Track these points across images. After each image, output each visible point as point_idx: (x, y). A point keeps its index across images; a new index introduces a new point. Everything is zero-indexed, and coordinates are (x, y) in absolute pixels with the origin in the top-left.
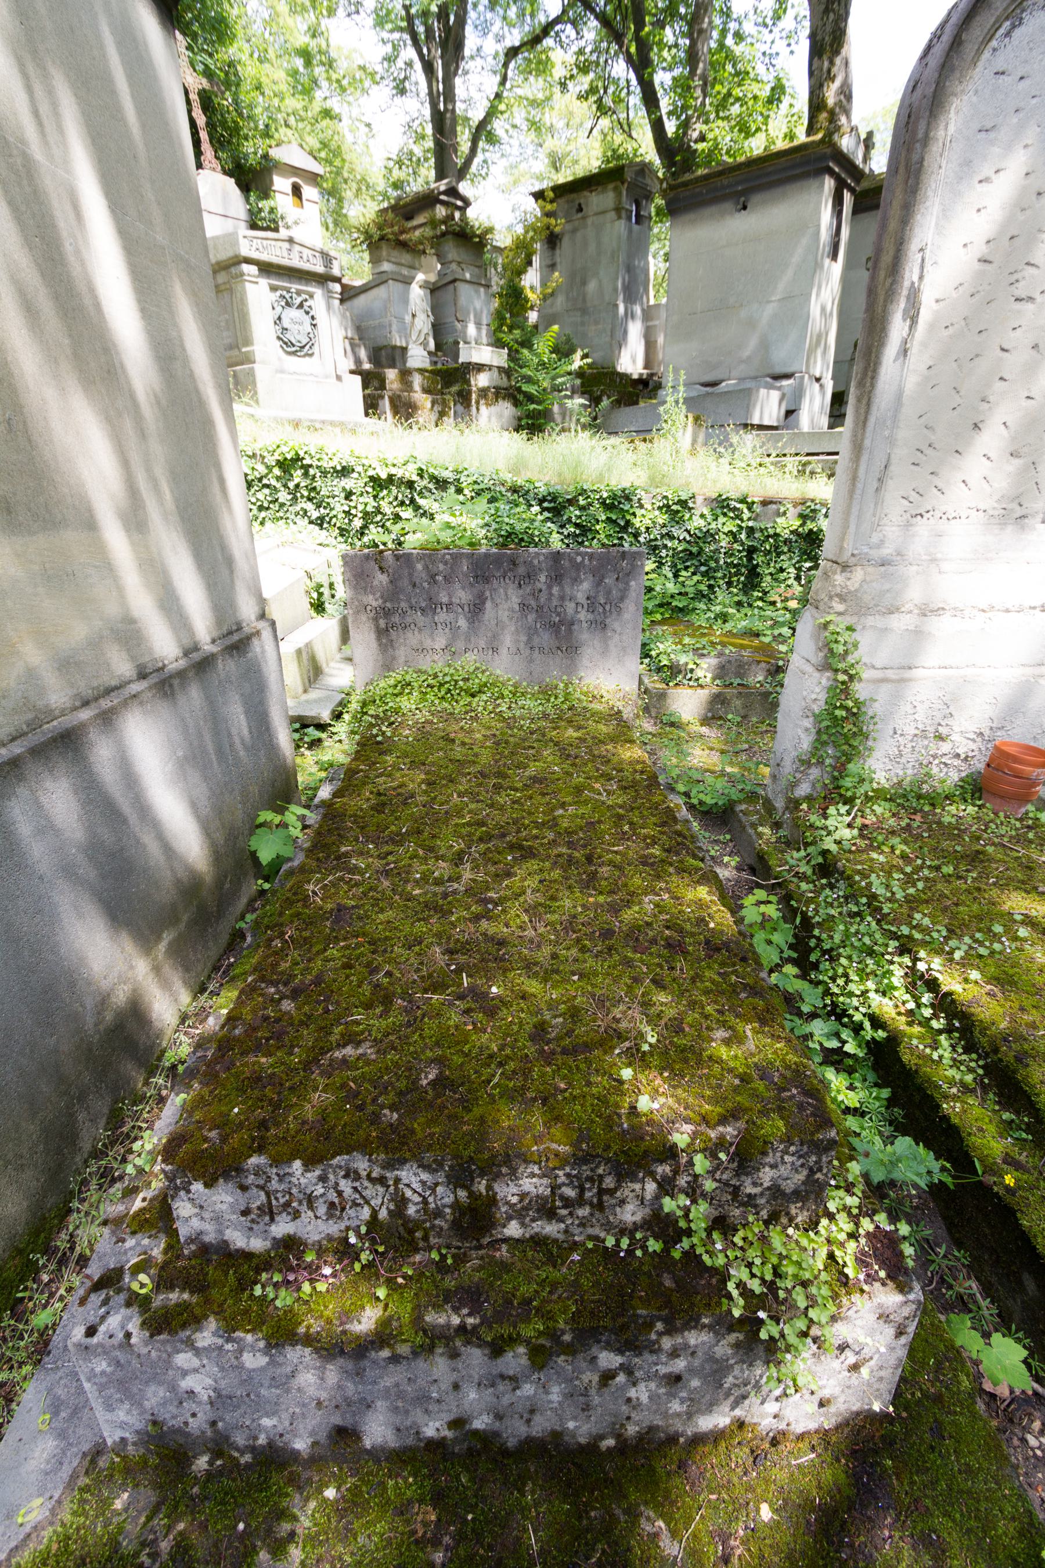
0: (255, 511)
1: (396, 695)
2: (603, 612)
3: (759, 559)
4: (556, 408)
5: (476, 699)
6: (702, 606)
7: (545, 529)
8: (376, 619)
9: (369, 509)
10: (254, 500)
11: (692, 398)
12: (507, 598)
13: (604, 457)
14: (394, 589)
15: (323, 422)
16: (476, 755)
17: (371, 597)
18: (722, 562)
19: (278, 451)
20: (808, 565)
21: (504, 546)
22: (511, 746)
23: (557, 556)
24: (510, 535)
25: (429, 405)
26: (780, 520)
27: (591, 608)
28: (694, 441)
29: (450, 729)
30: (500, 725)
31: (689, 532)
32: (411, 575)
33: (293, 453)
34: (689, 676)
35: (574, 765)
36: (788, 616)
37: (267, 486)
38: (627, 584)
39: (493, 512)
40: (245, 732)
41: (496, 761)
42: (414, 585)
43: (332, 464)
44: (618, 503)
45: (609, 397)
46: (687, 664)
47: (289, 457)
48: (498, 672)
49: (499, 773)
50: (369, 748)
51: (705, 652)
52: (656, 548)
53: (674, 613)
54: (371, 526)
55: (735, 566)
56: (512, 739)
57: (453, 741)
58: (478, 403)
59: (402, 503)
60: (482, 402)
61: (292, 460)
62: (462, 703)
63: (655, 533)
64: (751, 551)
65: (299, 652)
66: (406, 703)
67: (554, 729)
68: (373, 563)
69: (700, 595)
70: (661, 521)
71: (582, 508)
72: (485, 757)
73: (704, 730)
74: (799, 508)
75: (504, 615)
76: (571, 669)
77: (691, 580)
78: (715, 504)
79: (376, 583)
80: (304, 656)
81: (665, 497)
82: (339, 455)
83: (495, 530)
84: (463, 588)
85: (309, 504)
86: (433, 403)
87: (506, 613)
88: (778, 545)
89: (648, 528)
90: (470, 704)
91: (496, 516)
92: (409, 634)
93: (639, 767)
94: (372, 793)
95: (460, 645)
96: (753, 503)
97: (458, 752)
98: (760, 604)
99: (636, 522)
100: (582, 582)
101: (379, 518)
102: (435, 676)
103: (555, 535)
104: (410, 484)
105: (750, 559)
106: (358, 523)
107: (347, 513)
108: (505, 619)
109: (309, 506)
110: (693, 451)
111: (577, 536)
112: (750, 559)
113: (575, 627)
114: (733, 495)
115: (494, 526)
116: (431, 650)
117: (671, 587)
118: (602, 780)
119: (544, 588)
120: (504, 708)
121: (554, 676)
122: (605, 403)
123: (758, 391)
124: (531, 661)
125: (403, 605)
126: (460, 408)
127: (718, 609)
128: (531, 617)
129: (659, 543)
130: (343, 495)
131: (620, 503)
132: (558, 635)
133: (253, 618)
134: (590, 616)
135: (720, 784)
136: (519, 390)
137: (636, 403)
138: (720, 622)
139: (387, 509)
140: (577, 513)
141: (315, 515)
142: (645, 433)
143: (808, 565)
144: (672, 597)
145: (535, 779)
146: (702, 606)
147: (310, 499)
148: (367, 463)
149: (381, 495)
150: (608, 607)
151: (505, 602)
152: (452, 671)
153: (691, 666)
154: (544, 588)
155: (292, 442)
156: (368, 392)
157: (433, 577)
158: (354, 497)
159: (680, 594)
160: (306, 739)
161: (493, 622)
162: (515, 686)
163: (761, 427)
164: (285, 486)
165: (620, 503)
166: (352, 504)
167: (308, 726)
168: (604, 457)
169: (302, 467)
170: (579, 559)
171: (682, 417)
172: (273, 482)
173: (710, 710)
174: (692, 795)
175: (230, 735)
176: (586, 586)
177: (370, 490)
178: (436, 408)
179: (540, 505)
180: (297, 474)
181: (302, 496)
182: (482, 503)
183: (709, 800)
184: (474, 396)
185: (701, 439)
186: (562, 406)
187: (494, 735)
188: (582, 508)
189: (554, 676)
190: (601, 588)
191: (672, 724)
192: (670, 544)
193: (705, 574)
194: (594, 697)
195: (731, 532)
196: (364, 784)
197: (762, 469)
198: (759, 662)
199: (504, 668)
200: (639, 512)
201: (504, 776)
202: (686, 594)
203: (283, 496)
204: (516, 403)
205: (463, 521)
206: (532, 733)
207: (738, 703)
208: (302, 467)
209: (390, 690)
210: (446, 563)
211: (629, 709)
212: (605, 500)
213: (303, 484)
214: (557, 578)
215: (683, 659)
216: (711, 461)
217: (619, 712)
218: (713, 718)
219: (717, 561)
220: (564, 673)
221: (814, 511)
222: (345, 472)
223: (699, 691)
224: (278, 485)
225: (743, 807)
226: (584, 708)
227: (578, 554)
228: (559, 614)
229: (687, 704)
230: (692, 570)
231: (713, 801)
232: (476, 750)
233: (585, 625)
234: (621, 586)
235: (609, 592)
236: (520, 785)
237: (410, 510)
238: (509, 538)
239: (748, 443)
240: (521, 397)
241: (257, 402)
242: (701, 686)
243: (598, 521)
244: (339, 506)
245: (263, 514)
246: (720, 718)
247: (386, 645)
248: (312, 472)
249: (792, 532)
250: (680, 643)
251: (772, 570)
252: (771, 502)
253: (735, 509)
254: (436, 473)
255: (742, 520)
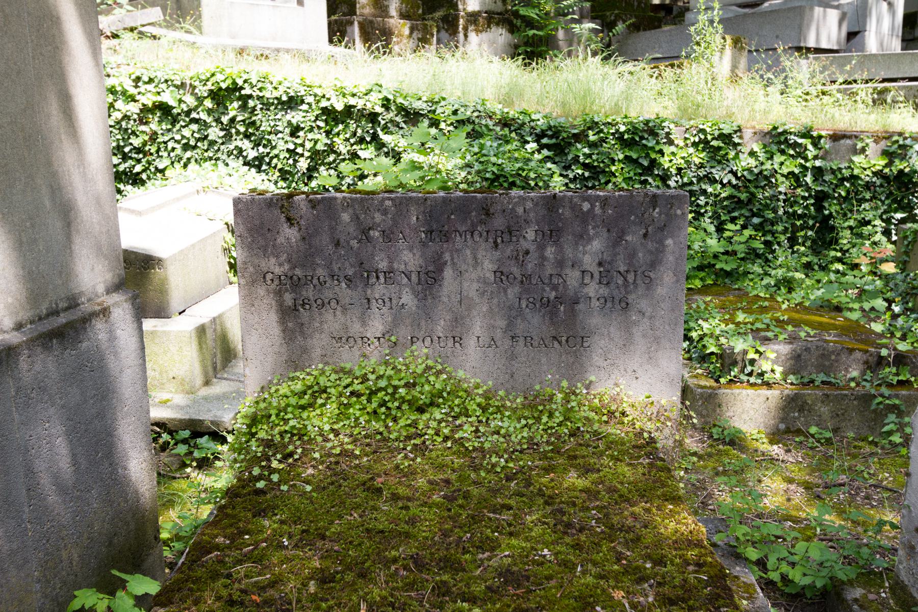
0: (179, 151)
1: (303, 408)
2: (623, 287)
3: (831, 208)
4: (561, 34)
5: (426, 416)
6: (757, 269)
7: (544, 171)
8: (279, 293)
9: (320, 147)
10: (178, 137)
11: (729, 19)
12: (476, 263)
13: (620, 86)
14: (305, 247)
15: (278, 50)
16: (412, 521)
17: (273, 260)
18: (781, 212)
19: (213, 80)
20: (899, 216)
21: (489, 190)
22: (476, 501)
23: (553, 201)
24: (497, 177)
25: (407, 31)
26: (857, 159)
27: (605, 278)
28: (734, 67)
29: (378, 468)
30: (458, 462)
31: (734, 174)
32: (332, 229)
33: (229, 82)
34: (749, 369)
35: (577, 546)
36: (879, 283)
37: (196, 121)
38: (661, 242)
39: (476, 149)
40: (64, 463)
41: (445, 534)
42: (337, 244)
43: (276, 94)
44: (641, 139)
45: (624, 21)
46: (745, 352)
47: (224, 86)
48: (461, 374)
49: (446, 559)
50: (243, 502)
51: (770, 334)
52: (692, 193)
53: (718, 278)
54: (322, 168)
55: (800, 217)
56: (475, 491)
57: (379, 491)
58: (466, 29)
59: (362, 140)
60: (471, 28)
61: (227, 89)
62: (402, 422)
63: (689, 176)
64: (821, 198)
65: (201, 331)
66: (319, 421)
67: (547, 470)
68: (277, 212)
69: (753, 255)
70: (697, 161)
71: (592, 145)
72: (428, 524)
73: (776, 450)
74: (883, 144)
75: (471, 289)
76: (575, 369)
77: (742, 236)
78: (768, 140)
79: (281, 240)
80: (210, 334)
81: (703, 131)
82: (287, 84)
83: (478, 172)
84: (411, 249)
85: (246, 141)
86: (412, 29)
87: (475, 286)
88: (857, 190)
89: (679, 170)
90: (414, 424)
91: (480, 155)
92: (329, 316)
93: (691, 554)
94: (219, 598)
95: (404, 332)
96: (820, 137)
97: (384, 513)
98: (840, 267)
99: (665, 162)
100: (590, 240)
101: (332, 158)
102: (365, 379)
103: (557, 178)
104: (373, 117)
105: (819, 208)
106: (303, 164)
107: (292, 152)
108: (473, 294)
109: (246, 145)
110: (734, 78)
111: (586, 179)
112: (819, 208)
113: (581, 306)
114: (792, 127)
115: (477, 166)
116: (367, 341)
117: (713, 243)
118: (627, 581)
119: (532, 248)
120: (467, 432)
121: (549, 380)
122: (620, 27)
123: (812, 9)
124: (513, 357)
125: (320, 272)
126: (444, 35)
127: (780, 273)
128: (513, 292)
129: (695, 188)
130: (288, 131)
131: (642, 138)
132: (555, 320)
133: (101, 289)
134: (604, 291)
135: (816, 551)
136: (516, 14)
137: (659, 27)
138: (783, 290)
139: (343, 148)
140: (586, 150)
141: (252, 154)
142: (673, 59)
143: (899, 216)
144: (715, 256)
145: (509, 576)
146: (757, 269)
147: (247, 136)
148: (319, 92)
149: (336, 130)
150: (631, 277)
151: (473, 271)
152: (390, 372)
153: (751, 355)
154: (532, 248)
155: (231, 70)
156: (333, 18)
157: (365, 232)
158: (301, 134)
159: (726, 253)
160: (197, 454)
161: (455, 299)
162: (487, 396)
163: (818, 51)
164: (218, 121)
165: (642, 138)
166: (299, 141)
167: (201, 435)
168: (620, 86)
169: (241, 98)
170: (586, 206)
171: (718, 38)
172: (203, 116)
173: (783, 420)
174: (770, 565)
175: (30, 472)
176: (596, 245)
177: (322, 124)
178: (414, 35)
179: (537, 141)
180: (233, 108)
181: (238, 133)
182: (460, 139)
183: (795, 575)
184: (461, 21)
185: (743, 62)
186: (568, 31)
187: (447, 482)
188: (592, 145)
189: (549, 380)
190: (620, 249)
191: (732, 443)
192: (710, 190)
193: (758, 228)
194: (611, 414)
195: (791, 173)
196: (215, 576)
197: (826, 98)
198: (851, 351)
199: (473, 366)
200: (668, 150)
201: (453, 566)
202: (734, 253)
203: (215, 133)
204: (512, 29)
205: (448, 162)
206: (509, 479)
207: (824, 410)
208: (241, 98)
209: (293, 401)
210: (385, 212)
211: (667, 432)
212: (622, 134)
213: (239, 118)
214: (552, 232)
215: (739, 345)
216: (758, 90)
217: (652, 441)
218: (788, 431)
219: (775, 211)
220: (563, 376)
221: (904, 147)
222: (292, 103)
223: (764, 392)
224: (209, 120)
225: (858, 592)
226: (596, 434)
227: (585, 199)
228: (555, 288)
229: (750, 411)
230: (741, 222)
231: (807, 581)
232: (414, 510)
233: (595, 304)
234: (650, 245)
235: (632, 256)
236: (478, 589)
237: (372, 148)
238: (498, 180)
239: (802, 70)
240: (518, 23)
241: (199, 28)
242: (768, 385)
243: (613, 161)
244: (282, 144)
245: (189, 154)
246: (799, 432)
247: (293, 331)
248: (251, 103)
249: (875, 174)
250: (732, 320)
251: (851, 223)
252: (844, 137)
253: (795, 145)
254: (406, 103)
255: (806, 160)
